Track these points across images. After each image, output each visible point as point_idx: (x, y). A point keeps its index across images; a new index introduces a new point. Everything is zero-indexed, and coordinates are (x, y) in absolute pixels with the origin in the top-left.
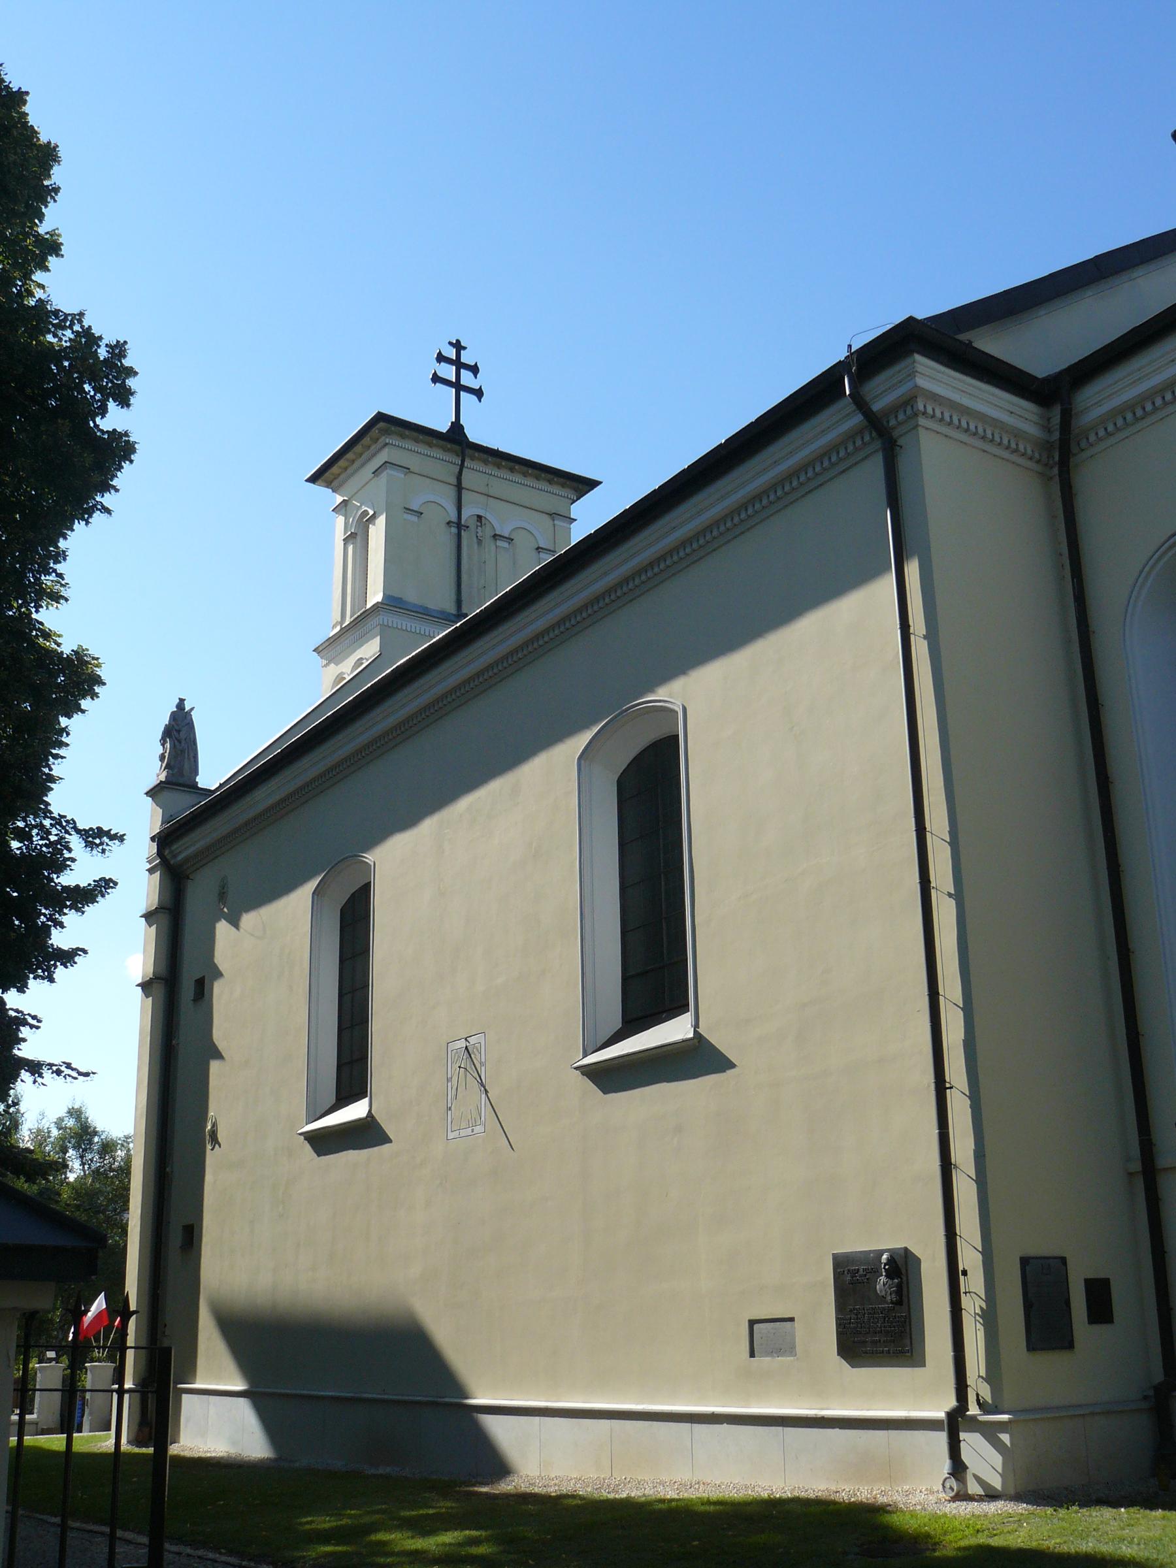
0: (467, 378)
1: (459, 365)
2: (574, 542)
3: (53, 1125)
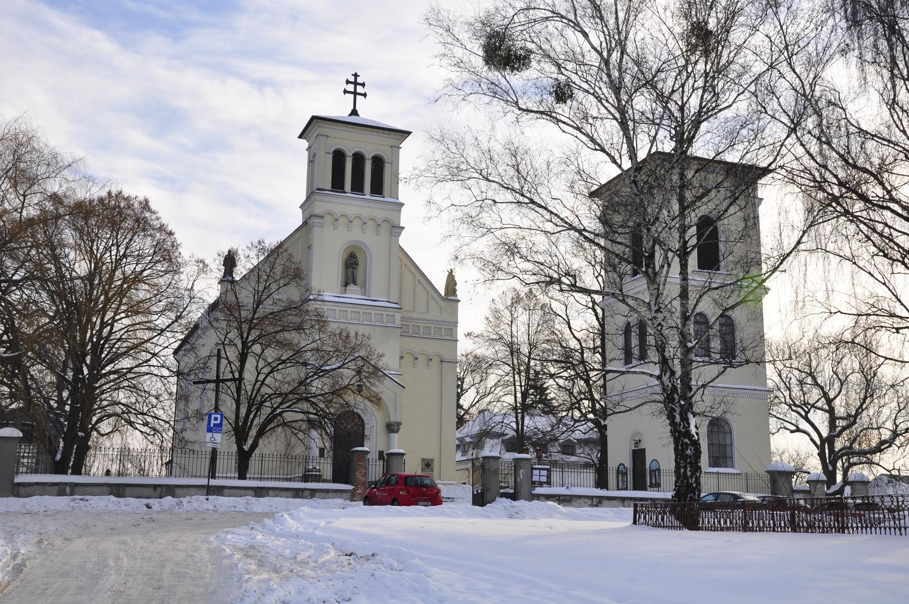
0: (360, 89)
1: (355, 83)
3: (122, 445)
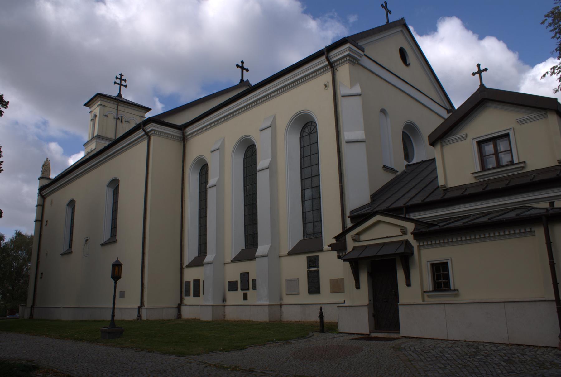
0: (123, 83)
1: (121, 79)
2: (70, 165)
